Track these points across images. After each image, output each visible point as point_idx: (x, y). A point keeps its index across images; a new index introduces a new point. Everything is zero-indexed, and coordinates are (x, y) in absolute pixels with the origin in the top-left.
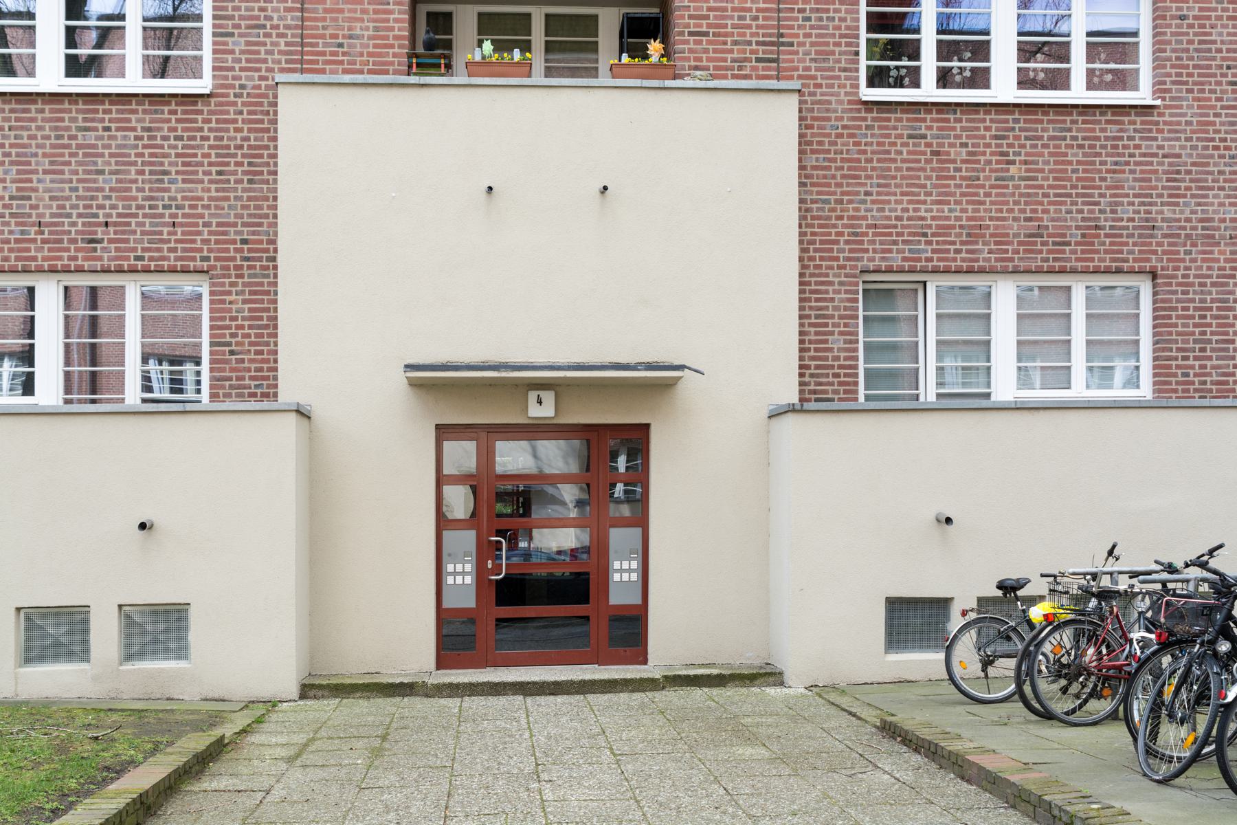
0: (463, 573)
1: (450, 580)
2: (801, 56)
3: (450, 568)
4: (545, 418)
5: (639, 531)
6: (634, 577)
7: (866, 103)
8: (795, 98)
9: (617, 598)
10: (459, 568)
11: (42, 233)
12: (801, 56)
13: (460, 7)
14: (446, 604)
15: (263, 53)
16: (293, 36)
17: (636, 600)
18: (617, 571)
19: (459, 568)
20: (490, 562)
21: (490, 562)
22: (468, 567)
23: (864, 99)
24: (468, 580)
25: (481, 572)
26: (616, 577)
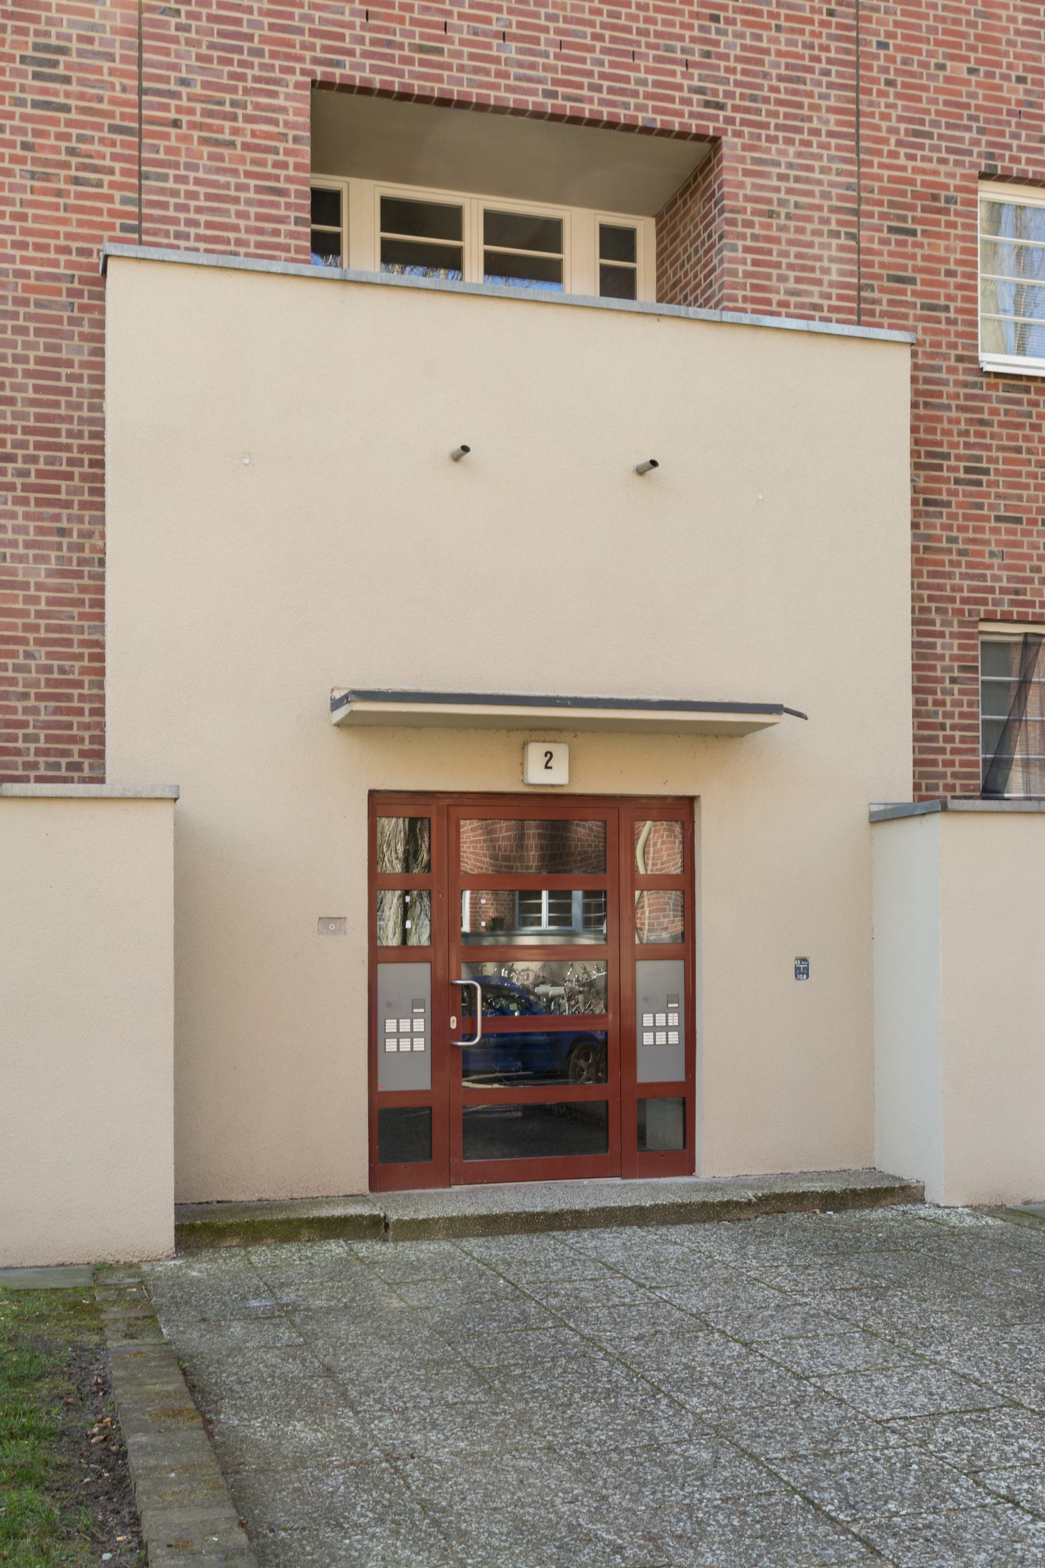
0: (412, 1035)
1: (391, 1045)
2: (75, 538)
3: (390, 1026)
4: (552, 786)
5: (679, 965)
6: (674, 1038)
7: (988, 374)
8: (907, 352)
9: (646, 1073)
10: (405, 1026)
11: (691, 77)
12: (75, 538)
13: (355, 182)
14: (386, 1084)
15: (227, 131)
16: (124, 172)
17: (678, 1075)
18: (648, 1029)
19: (405, 1026)
20: (453, 1019)
21: (453, 1019)
22: (420, 1025)
23: (988, 368)
24: (420, 1044)
25: (438, 1033)
26: (647, 1039)
